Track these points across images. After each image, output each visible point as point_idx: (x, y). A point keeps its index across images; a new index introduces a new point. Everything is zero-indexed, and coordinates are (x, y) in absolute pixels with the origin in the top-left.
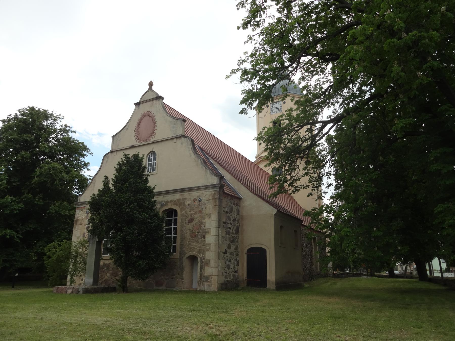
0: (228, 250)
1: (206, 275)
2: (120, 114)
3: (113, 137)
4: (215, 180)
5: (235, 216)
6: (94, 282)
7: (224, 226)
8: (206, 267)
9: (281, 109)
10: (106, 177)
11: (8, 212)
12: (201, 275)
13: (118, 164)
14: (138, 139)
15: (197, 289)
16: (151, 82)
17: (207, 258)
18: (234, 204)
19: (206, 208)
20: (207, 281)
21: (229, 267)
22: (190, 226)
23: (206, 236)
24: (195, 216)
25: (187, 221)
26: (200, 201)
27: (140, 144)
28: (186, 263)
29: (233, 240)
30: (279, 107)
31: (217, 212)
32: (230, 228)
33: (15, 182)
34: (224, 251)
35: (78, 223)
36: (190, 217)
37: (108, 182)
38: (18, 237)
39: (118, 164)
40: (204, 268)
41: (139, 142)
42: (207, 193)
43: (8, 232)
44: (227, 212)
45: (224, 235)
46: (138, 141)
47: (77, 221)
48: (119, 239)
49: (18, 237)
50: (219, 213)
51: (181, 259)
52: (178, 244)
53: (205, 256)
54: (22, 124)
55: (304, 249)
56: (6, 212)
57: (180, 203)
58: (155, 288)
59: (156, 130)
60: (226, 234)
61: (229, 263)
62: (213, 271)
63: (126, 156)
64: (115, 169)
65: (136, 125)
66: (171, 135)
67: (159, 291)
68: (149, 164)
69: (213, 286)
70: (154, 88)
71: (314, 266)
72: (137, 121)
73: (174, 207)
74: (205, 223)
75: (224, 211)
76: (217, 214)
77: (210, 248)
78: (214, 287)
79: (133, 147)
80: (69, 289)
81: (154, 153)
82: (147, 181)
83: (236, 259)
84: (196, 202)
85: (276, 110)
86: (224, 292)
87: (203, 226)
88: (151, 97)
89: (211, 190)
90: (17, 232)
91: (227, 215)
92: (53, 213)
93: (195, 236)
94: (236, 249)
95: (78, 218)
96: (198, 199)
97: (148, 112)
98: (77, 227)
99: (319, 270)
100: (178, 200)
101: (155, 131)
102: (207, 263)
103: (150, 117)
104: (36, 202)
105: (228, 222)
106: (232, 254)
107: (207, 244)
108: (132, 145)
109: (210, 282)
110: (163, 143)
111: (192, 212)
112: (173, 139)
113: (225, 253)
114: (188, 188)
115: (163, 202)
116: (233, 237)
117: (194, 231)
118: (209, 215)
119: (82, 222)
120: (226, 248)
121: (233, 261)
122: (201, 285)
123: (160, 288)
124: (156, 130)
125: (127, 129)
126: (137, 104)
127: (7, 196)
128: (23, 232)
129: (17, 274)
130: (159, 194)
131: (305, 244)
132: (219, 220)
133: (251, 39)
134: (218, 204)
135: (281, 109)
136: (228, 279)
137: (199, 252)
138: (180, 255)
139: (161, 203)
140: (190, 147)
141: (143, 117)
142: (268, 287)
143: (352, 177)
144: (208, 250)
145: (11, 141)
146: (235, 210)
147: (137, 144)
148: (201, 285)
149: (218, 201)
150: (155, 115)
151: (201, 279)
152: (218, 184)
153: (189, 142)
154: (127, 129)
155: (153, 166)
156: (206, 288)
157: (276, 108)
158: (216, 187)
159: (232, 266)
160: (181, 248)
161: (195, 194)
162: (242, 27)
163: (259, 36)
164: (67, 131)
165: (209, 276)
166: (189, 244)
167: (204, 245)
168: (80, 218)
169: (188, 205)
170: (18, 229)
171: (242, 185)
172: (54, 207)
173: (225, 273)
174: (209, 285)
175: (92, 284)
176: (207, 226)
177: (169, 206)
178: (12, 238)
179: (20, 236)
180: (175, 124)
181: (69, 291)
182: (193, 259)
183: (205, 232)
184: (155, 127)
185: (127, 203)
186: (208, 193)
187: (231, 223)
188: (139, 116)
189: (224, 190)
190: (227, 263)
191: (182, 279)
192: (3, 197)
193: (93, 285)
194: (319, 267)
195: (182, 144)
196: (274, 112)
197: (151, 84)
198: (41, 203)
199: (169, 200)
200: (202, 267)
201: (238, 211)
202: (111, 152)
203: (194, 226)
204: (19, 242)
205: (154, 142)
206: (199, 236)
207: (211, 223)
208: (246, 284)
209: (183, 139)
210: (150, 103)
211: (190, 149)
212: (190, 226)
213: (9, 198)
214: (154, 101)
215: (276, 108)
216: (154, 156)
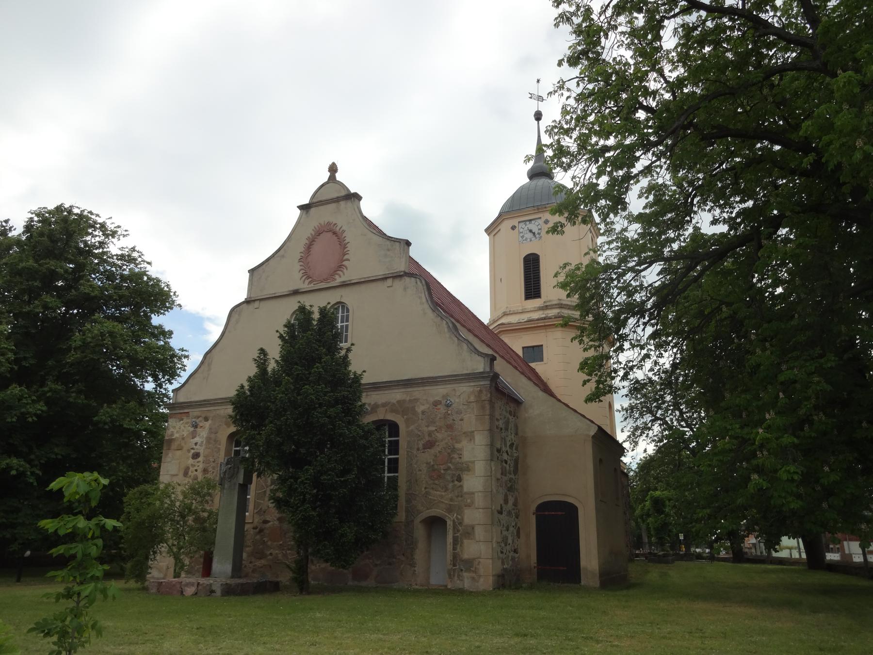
0: (504, 507)
1: (466, 556)
3: (252, 271)
4: (479, 365)
8: (465, 541)
9: (539, 234)
10: (262, 351)
11: (14, 420)
12: (455, 557)
13: (285, 326)
14: (309, 277)
15: (446, 586)
17: (467, 520)
19: (462, 420)
20: (468, 570)
22: (427, 457)
23: (465, 477)
24: (439, 436)
25: (421, 446)
26: (448, 406)
27: (312, 287)
28: (420, 532)
29: (511, 487)
30: (535, 230)
31: (487, 427)
33: (25, 358)
35: (174, 446)
36: (427, 438)
37: (265, 361)
38: (32, 473)
39: (285, 326)
40: (462, 543)
41: (310, 283)
42: (465, 389)
43: (15, 461)
44: (501, 429)
45: (499, 476)
46: (307, 281)
47: (171, 441)
48: (306, 479)
49: (32, 473)
50: (491, 430)
51: (409, 523)
52: (402, 492)
53: (463, 519)
54: (45, 238)
56: (9, 420)
57: (402, 407)
58: (350, 583)
59: (348, 260)
60: (502, 474)
62: (481, 549)
63: (302, 309)
64: (278, 334)
65: (302, 250)
66: (381, 272)
67: (360, 591)
69: (482, 580)
70: (339, 177)
72: (304, 241)
73: (390, 417)
74: (461, 450)
76: (486, 433)
77: (473, 502)
78: (486, 582)
79: (296, 292)
80: (187, 585)
81: (343, 307)
82: (345, 361)
84: (439, 407)
85: (530, 235)
86: (506, 592)
87: (456, 456)
88: (335, 195)
89: (472, 384)
90: (29, 462)
92: (105, 423)
93: (440, 476)
94: (515, 504)
95: (172, 435)
96: (444, 402)
97: (329, 224)
98: (170, 455)
100: (398, 402)
101: (345, 263)
102: (469, 533)
103: (334, 233)
104: (71, 400)
105: (504, 449)
107: (466, 493)
108: (295, 288)
109: (475, 572)
110: (363, 287)
111: (432, 428)
112: (386, 278)
113: (500, 512)
114: (423, 379)
117: (436, 467)
118: (470, 436)
119: (183, 444)
120: (502, 502)
121: (511, 529)
122: (456, 578)
123: (364, 584)
124: (348, 260)
125: (283, 256)
126: (303, 208)
127: (14, 385)
128: (42, 461)
129: (28, 553)
130: (376, 387)
132: (492, 445)
133: (561, 87)
134: (488, 412)
135: (539, 234)
137: (450, 510)
138: (407, 516)
139: (375, 405)
140: (424, 296)
141: (319, 233)
142: (583, 583)
143: (779, 364)
144: (469, 506)
145: (20, 273)
146: (511, 425)
147: (305, 286)
148: (456, 578)
149: (488, 406)
150: (344, 231)
151: (454, 565)
152: (488, 372)
153: (420, 286)
154: (283, 256)
156: (467, 584)
157: (531, 231)
158: (483, 377)
160: (408, 501)
161: (439, 391)
162: (568, 61)
163: (578, 85)
164: (133, 260)
165: (474, 559)
166: (427, 493)
167: (461, 495)
168: (176, 435)
169: (423, 412)
170: (32, 457)
171: (522, 376)
172: (106, 413)
174: (473, 578)
175: (230, 574)
176: (467, 457)
178: (21, 474)
179: (38, 472)
180: (388, 250)
181: (190, 591)
182: (435, 524)
183: (462, 470)
184: (344, 255)
185: (321, 405)
186: (465, 390)
188: (309, 232)
191: (413, 565)
192: (7, 387)
193: (233, 577)
195: (405, 289)
196: (526, 239)
197: (333, 169)
198: (81, 400)
199: (380, 403)
200: (456, 541)
201: (516, 427)
202: (247, 302)
203: (436, 456)
204: (35, 484)
205: (344, 285)
206: (449, 478)
207: (475, 451)
208: (535, 577)
209: (407, 280)
210: (333, 206)
211: (424, 300)
212: (427, 457)
213: (15, 390)
214: (342, 203)
215: (531, 231)
216: (343, 312)
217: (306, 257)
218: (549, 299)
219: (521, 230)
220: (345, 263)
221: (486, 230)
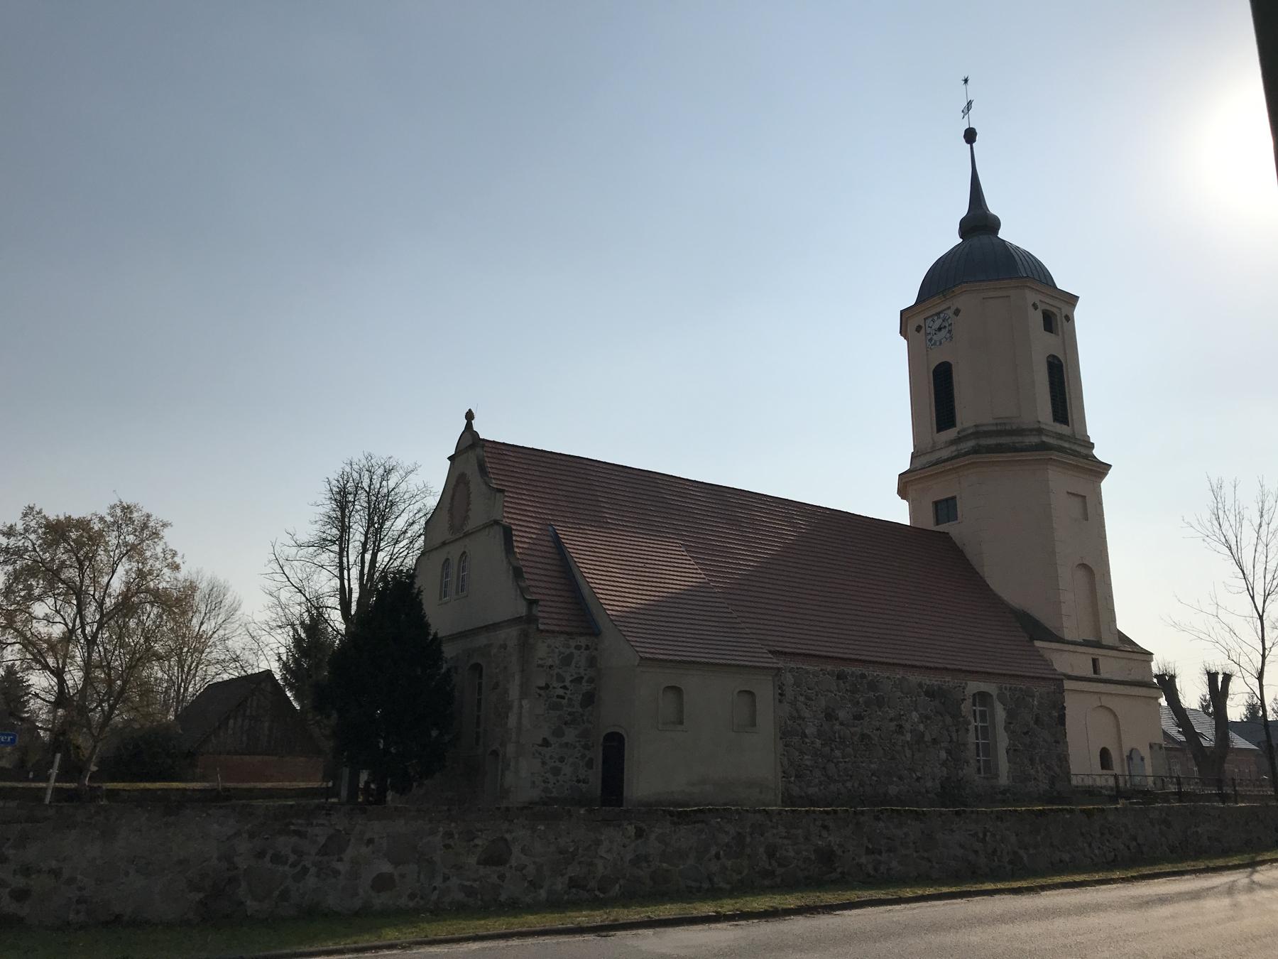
34: (540, 742)
44: (551, 667)
61: (558, 764)
83: (583, 756)
113: (546, 743)
187: (565, 687)
197: (470, 416)
217: (450, 510)
219: (929, 330)
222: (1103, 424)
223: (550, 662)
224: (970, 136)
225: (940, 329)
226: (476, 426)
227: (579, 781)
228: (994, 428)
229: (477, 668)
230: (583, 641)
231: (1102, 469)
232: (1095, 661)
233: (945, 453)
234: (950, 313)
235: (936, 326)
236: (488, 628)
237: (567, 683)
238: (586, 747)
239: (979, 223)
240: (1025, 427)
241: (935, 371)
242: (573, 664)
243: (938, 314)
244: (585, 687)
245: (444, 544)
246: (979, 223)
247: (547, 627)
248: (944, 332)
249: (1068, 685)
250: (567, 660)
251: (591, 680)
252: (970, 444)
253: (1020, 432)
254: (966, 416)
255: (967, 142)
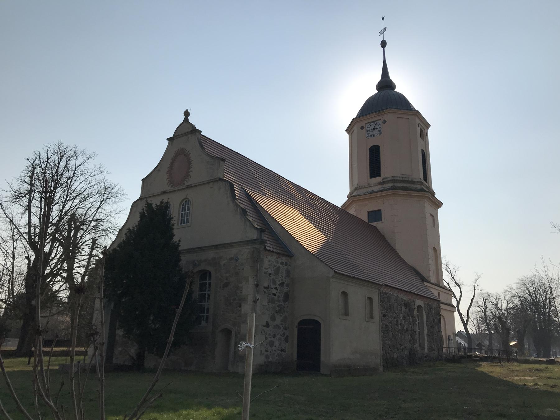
2: (150, 153)
4: (254, 235)
5: (283, 278)
6: (300, 355)
7: (265, 292)
14: (171, 184)
16: (187, 110)
18: (282, 263)
21: (271, 344)
26: (237, 260)
32: (274, 295)
34: (265, 324)
41: (172, 186)
44: (270, 274)
55: (399, 322)
60: (269, 302)
61: (272, 339)
65: (169, 166)
68: (182, 214)
71: (417, 345)
75: (265, 273)
79: (164, 192)
83: (284, 334)
91: (272, 278)
99: (426, 351)
101: (190, 173)
105: (272, 286)
106: (277, 327)
108: (163, 190)
111: (228, 275)
112: (210, 182)
113: (267, 325)
115: (196, 262)
116: (278, 306)
121: (278, 336)
124: (191, 171)
125: (159, 171)
131: (401, 315)
136: (271, 359)
147: (168, 189)
150: (190, 154)
154: (159, 171)
155: (187, 216)
159: (277, 343)
161: (233, 252)
169: (224, 265)
173: (266, 351)
177: (203, 267)
182: (228, 333)
187: (276, 288)
189: (265, 246)
190: (269, 339)
194: (426, 345)
196: (371, 135)
197: (187, 114)
205: (189, 187)
211: (228, 195)
217: (170, 172)
218: (386, 176)
219: (368, 129)
220: (190, 173)
221: (347, 131)
222: (439, 184)
223: (269, 271)
224: (384, 44)
225: (374, 129)
226: (191, 120)
227: (282, 351)
228: (401, 179)
229: (205, 275)
230: (284, 259)
231: (439, 204)
232: (439, 293)
233: (376, 189)
234: (380, 122)
235: (372, 127)
236: (216, 247)
237: (277, 286)
238: (285, 329)
239: (386, 84)
240: (414, 180)
241: (370, 149)
242: (280, 275)
243: (374, 122)
244: (285, 289)
245: (164, 192)
246: (386, 84)
247: (270, 249)
248: (376, 131)
249: (442, 306)
250: (277, 271)
251: (288, 285)
252: (390, 185)
253: (413, 182)
254: (387, 171)
255: (382, 47)
